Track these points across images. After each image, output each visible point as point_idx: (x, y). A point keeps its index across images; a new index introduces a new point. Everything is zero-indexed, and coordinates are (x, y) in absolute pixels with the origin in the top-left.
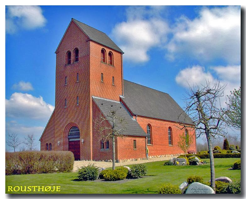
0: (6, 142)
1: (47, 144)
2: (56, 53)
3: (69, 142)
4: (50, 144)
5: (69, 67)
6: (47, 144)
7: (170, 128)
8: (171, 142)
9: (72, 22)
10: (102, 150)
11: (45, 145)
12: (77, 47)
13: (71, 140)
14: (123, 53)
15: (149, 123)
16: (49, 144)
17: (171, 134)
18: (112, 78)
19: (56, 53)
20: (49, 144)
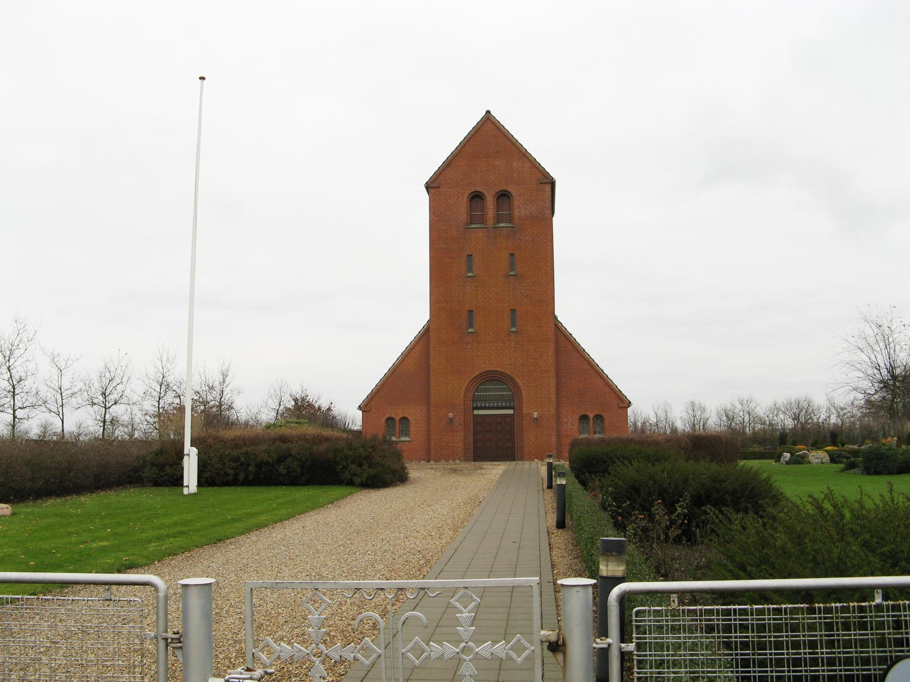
4: (404, 420)
11: (384, 420)
13: (476, 412)
16: (591, 418)
19: (428, 187)
20: (591, 418)
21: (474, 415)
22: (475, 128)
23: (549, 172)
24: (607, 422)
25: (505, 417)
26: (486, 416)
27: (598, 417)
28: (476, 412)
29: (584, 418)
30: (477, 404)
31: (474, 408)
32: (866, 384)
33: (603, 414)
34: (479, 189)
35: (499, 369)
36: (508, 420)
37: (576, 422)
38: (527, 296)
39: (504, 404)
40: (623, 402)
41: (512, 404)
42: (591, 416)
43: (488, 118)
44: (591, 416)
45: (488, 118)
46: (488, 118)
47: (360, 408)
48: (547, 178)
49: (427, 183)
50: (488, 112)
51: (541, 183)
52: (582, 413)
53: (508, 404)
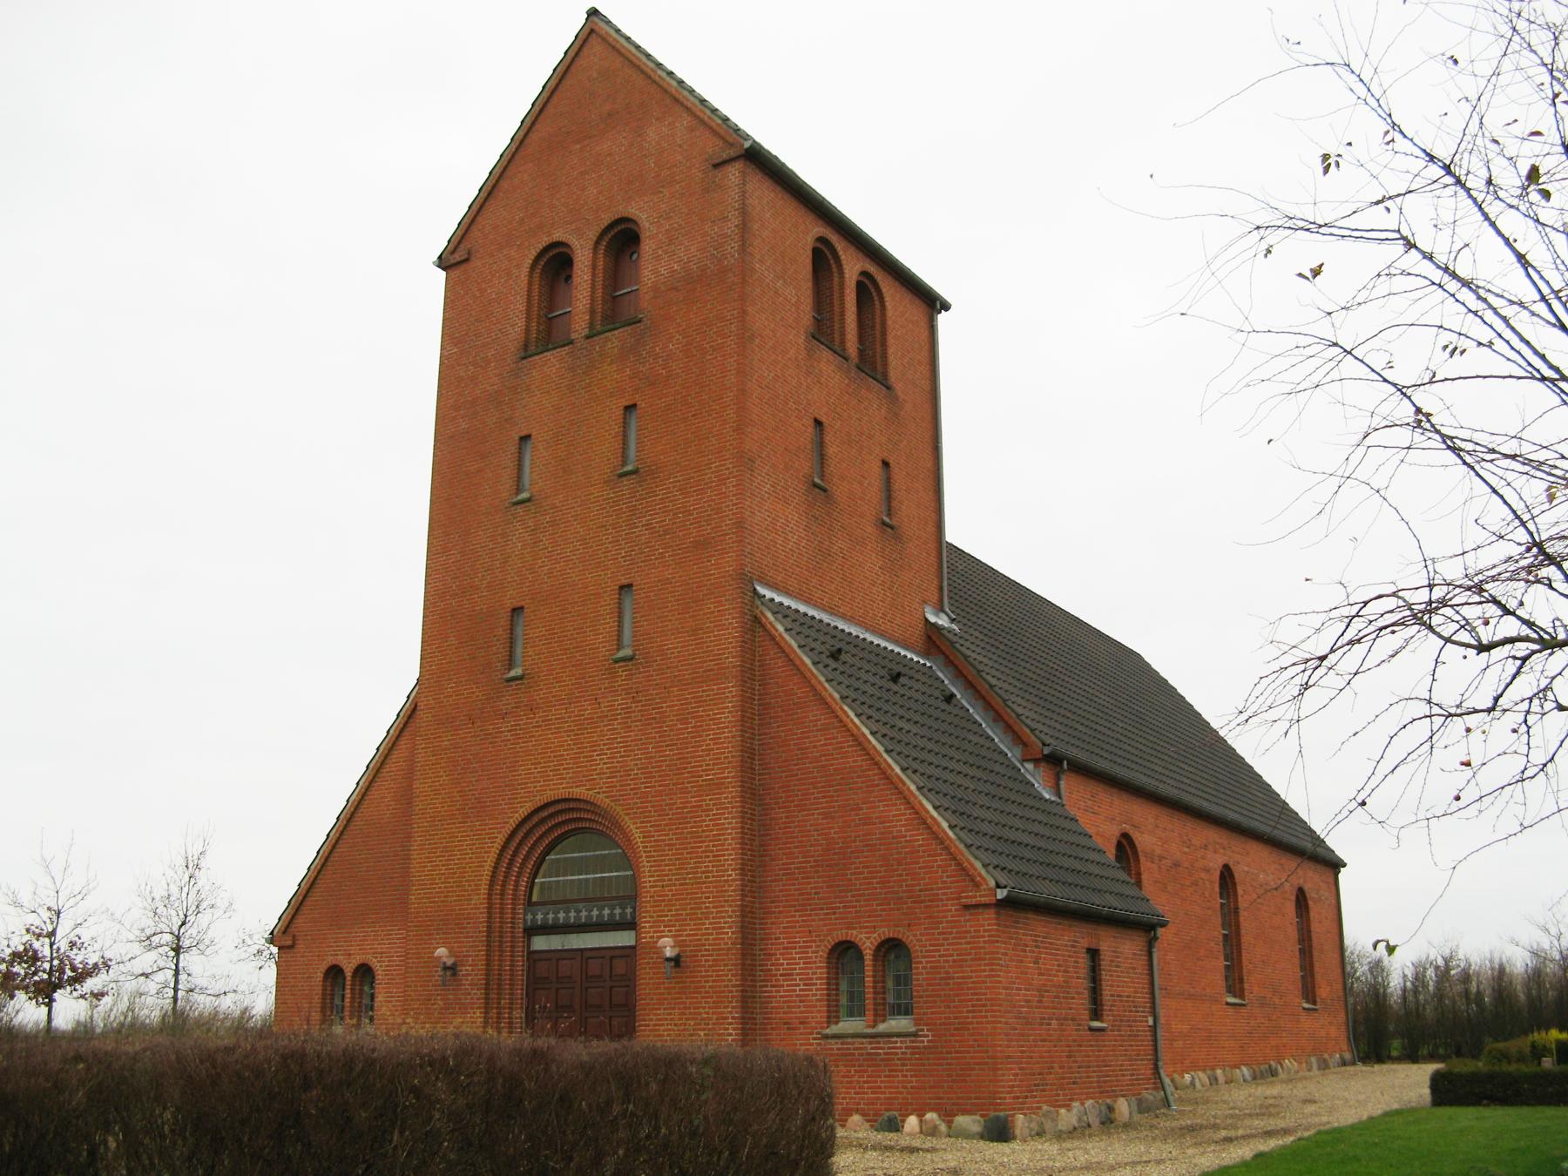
0: (422, 658)
1: (334, 972)
2: (443, 262)
3: (533, 957)
4: (365, 972)
5: (552, 363)
6: (334, 972)
7: (1227, 878)
8: (1235, 982)
9: (593, 40)
10: (848, 1025)
11: (320, 975)
12: (632, 211)
13: (540, 943)
14: (946, 307)
15: (1126, 827)
16: (348, 974)
17: (1230, 915)
18: (876, 467)
19: (443, 262)
20: (348, 974)
21: (530, 953)
22: (558, 70)
23: (1297, 810)
24: (921, 973)
25: (612, 958)
26: (617, 952)
27: (892, 948)
28: (540, 943)
29: (844, 952)
30: (534, 915)
31: (532, 931)
32: (1359, 948)
33: (910, 938)
34: (558, 236)
35: (578, 792)
36: (620, 967)
37: (819, 972)
38: (666, 532)
39: (561, 915)
40: (977, 885)
41: (629, 910)
42: (868, 943)
43: (596, 29)
44: (868, 943)
45: (596, 29)
46: (592, 31)
47: (272, 939)
48: (732, 145)
49: (440, 257)
50: (593, 13)
51: (716, 166)
52: (840, 935)
53: (618, 911)
